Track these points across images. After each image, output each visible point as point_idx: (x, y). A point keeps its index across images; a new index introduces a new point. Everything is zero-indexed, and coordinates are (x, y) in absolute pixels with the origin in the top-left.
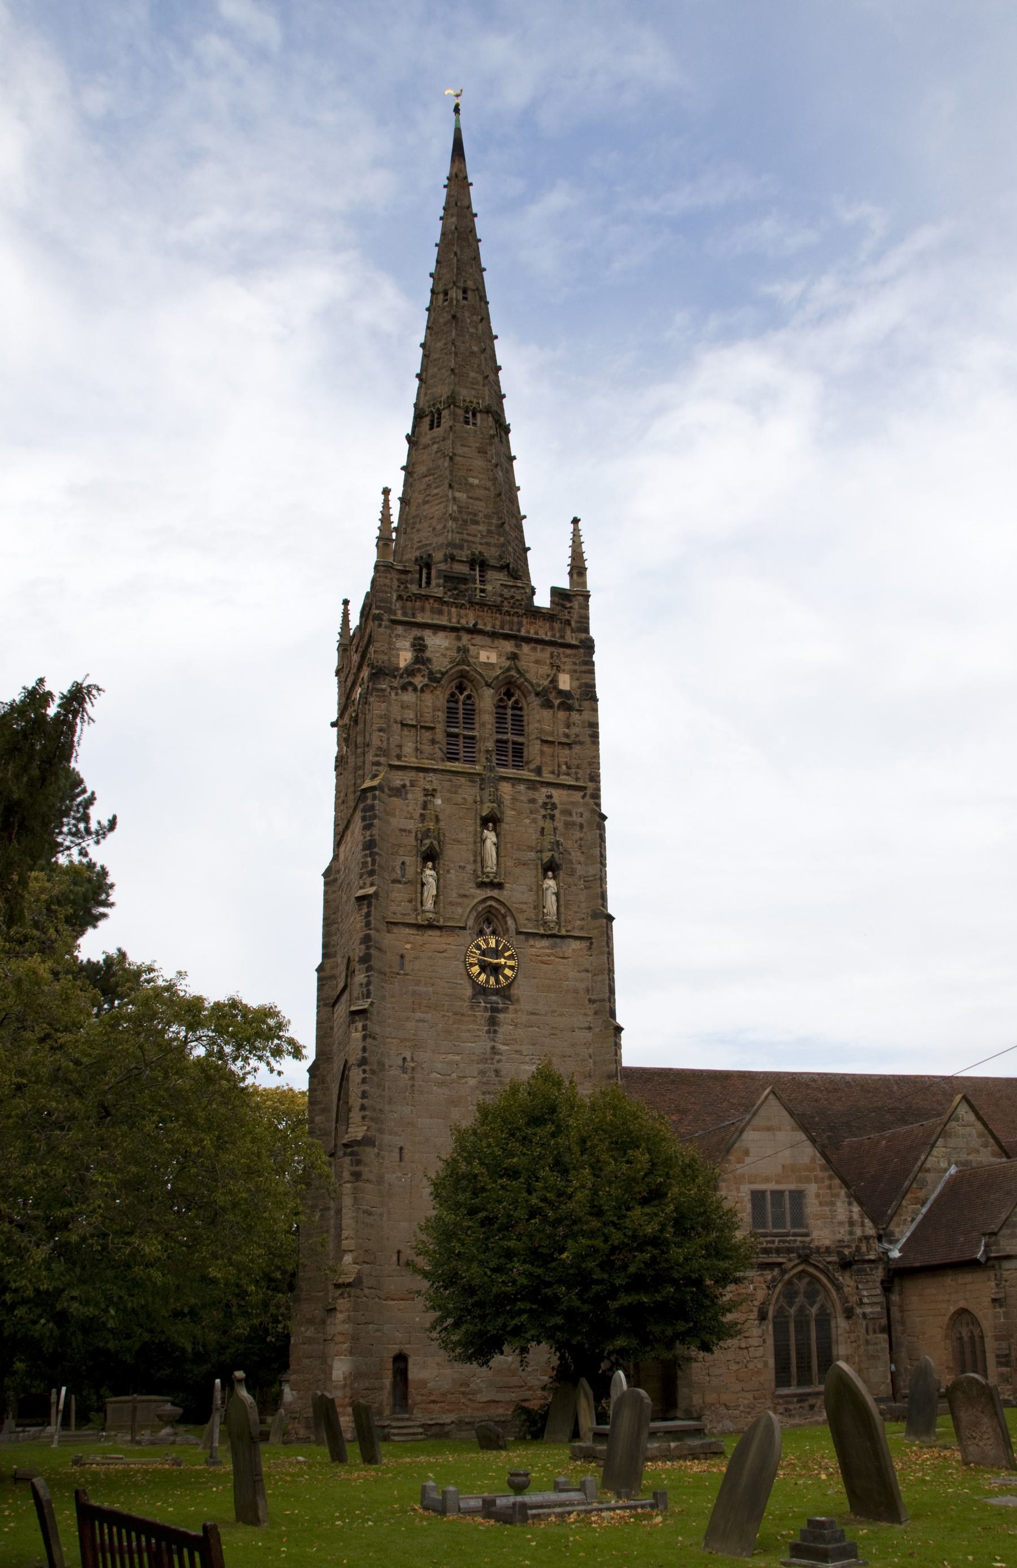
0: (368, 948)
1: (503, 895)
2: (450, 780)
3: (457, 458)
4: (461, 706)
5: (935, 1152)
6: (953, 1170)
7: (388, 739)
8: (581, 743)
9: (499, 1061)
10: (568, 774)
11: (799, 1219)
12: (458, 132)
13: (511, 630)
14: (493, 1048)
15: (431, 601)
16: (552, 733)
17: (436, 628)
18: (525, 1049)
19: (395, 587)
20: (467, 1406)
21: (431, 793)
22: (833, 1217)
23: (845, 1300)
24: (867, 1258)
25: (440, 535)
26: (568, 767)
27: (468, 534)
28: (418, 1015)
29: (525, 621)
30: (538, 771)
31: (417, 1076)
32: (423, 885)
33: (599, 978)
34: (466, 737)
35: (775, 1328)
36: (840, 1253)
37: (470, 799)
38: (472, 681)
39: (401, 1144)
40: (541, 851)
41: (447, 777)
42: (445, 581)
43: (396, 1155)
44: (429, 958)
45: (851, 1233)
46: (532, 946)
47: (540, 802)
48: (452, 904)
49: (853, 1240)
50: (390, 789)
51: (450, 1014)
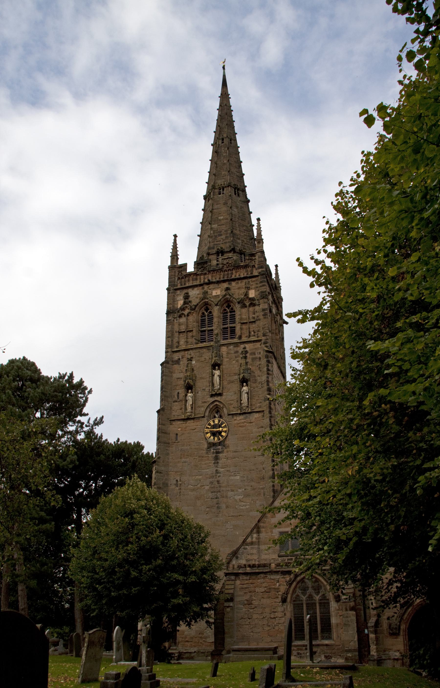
4: (206, 317)
8: (259, 320)
10: (254, 336)
12: (224, 76)
14: (217, 470)
17: (193, 287)
18: (232, 469)
19: (177, 275)
20: (203, 644)
21: (190, 360)
26: (254, 332)
28: (183, 460)
30: (240, 337)
34: (209, 331)
37: (207, 358)
41: (197, 351)
44: (189, 433)
46: (235, 420)
47: (240, 351)
48: (199, 407)
50: (172, 361)
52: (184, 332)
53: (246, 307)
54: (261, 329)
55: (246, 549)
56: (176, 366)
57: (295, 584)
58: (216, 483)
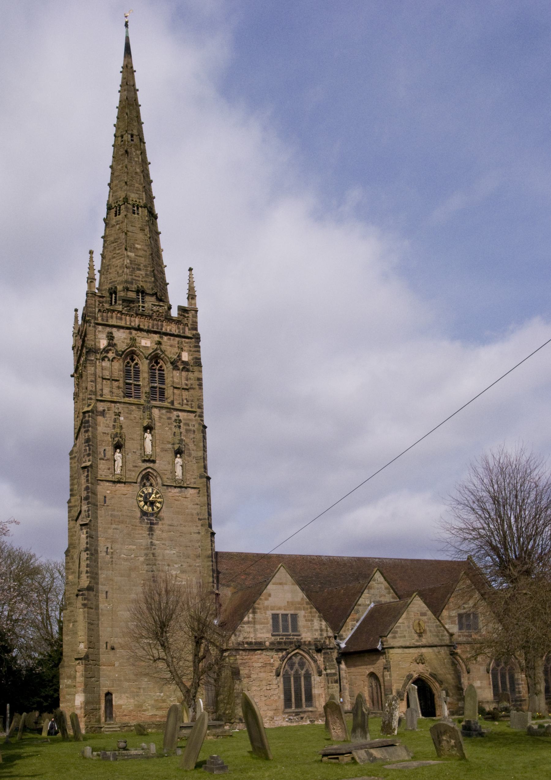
0: (88, 493)
1: (156, 466)
2: (128, 408)
3: (129, 233)
4: (132, 368)
5: (363, 596)
6: (372, 605)
7: (96, 386)
8: (193, 389)
9: (154, 549)
10: (187, 405)
11: (295, 627)
12: (127, 39)
13: (158, 329)
14: (151, 542)
15: (116, 312)
16: (178, 383)
17: (119, 327)
18: (167, 543)
21: (119, 414)
22: (313, 627)
23: (318, 667)
24: (329, 647)
25: (121, 276)
26: (187, 401)
27: (135, 276)
29: (164, 324)
30: (172, 403)
31: (114, 556)
32: (115, 461)
33: (204, 508)
35: (284, 680)
36: (315, 644)
37: (138, 417)
38: (137, 356)
39: (107, 590)
40: (173, 444)
42: (123, 302)
43: (104, 595)
45: (321, 635)
47: (173, 419)
48: (130, 470)
49: (322, 639)
51: (129, 526)
52: (109, 379)
53: (179, 370)
54: (196, 400)
55: (244, 627)
56: (100, 419)
57: (286, 660)
58: (151, 555)
